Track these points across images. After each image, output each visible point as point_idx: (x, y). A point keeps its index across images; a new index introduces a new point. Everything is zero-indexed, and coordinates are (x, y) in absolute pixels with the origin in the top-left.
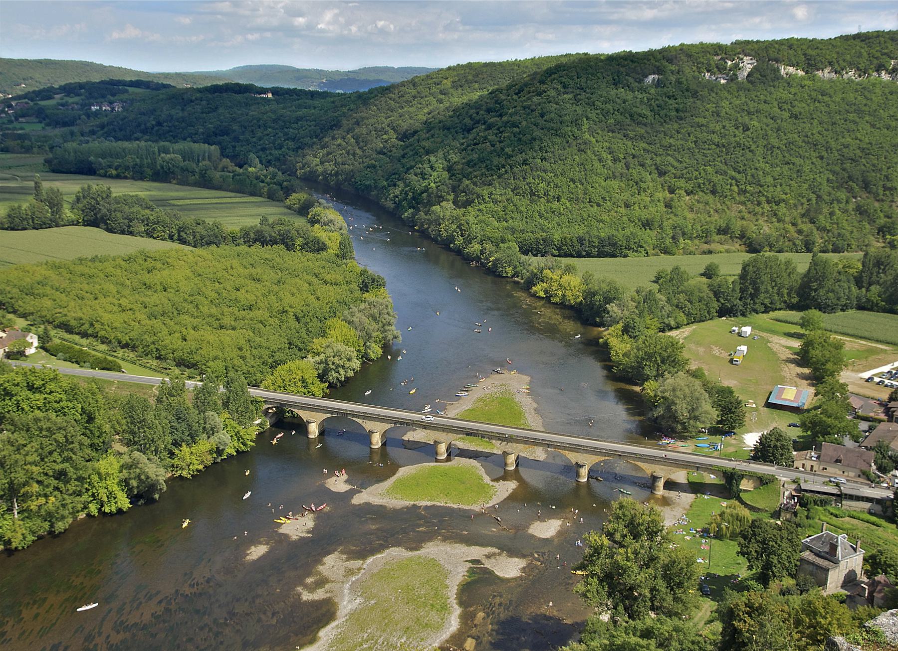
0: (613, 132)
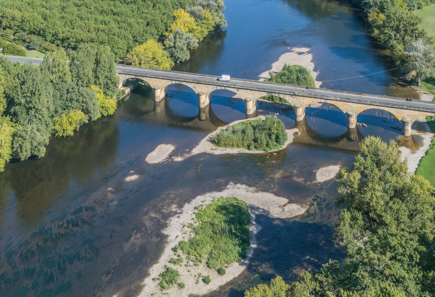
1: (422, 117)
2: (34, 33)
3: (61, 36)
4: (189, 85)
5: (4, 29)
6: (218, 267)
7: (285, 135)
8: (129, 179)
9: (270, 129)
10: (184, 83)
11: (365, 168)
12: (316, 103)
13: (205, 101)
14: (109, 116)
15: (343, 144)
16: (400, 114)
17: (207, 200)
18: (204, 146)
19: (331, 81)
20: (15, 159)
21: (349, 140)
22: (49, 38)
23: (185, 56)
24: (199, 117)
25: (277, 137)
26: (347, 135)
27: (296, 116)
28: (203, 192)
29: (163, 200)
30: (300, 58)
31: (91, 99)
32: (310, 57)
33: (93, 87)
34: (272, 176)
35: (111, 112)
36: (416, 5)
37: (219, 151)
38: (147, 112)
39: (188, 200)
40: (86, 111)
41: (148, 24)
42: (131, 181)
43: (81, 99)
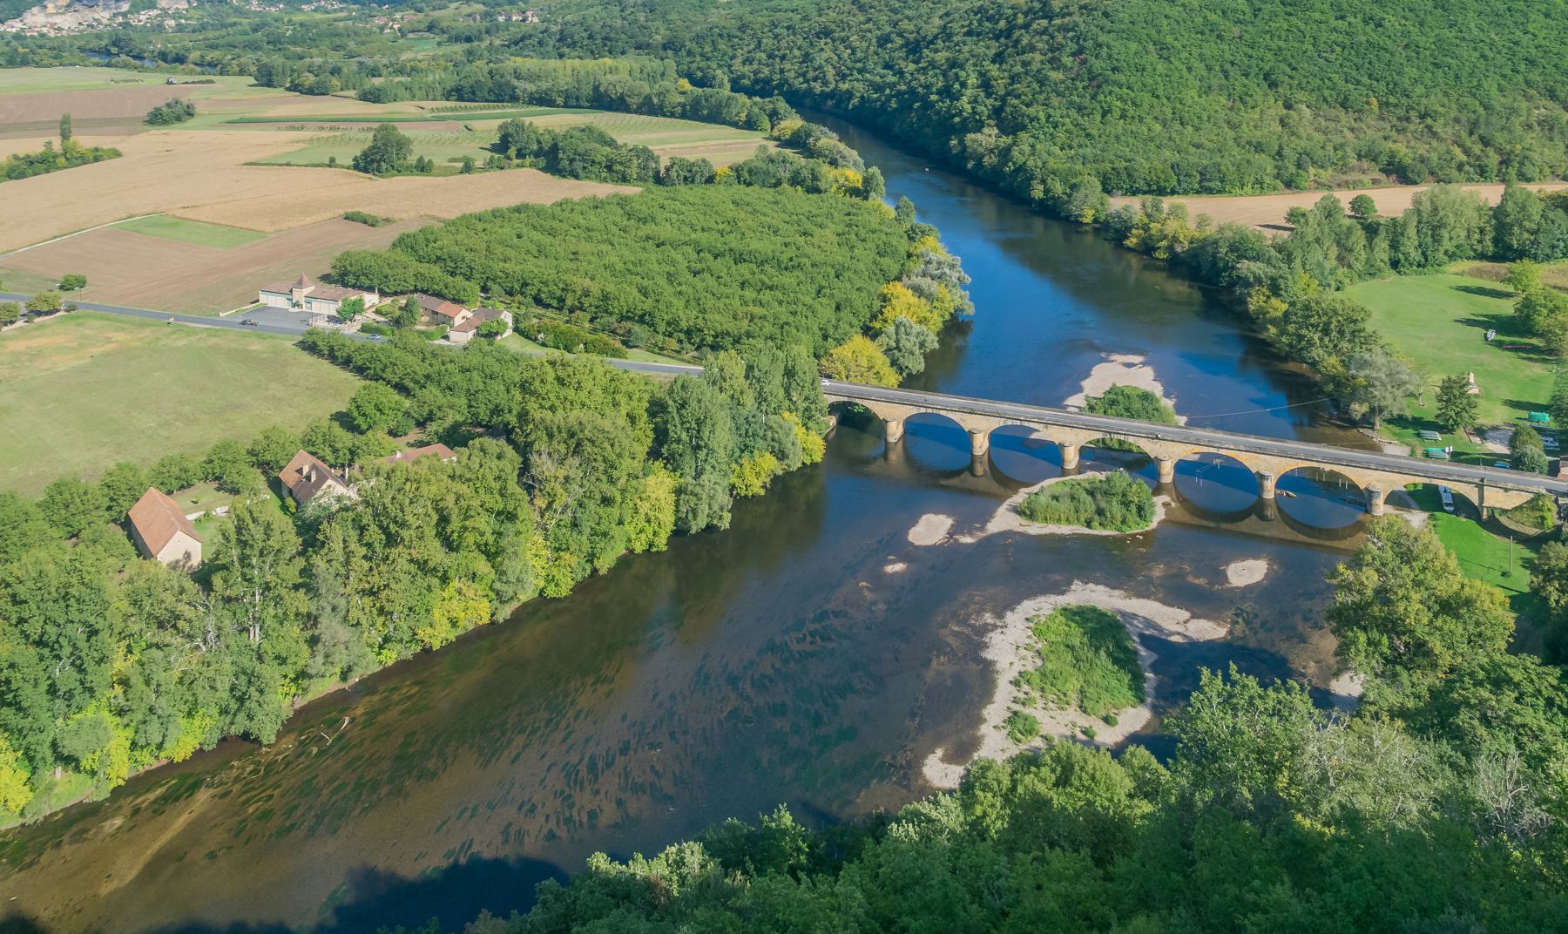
0: (1202, 33)
1: (1400, 482)
2: (629, 318)
3: (684, 325)
4: (951, 415)
5: (571, 311)
6: (1104, 713)
7: (1152, 505)
8: (890, 569)
9: (1124, 495)
10: (942, 413)
11: (1383, 565)
12: (1188, 452)
13: (981, 445)
14: (814, 465)
15: (1251, 524)
16: (1362, 478)
17: (1044, 606)
18: (1003, 520)
19: (1199, 413)
20: (679, 532)
21: (1263, 517)
22: (662, 327)
23: (917, 365)
24: (971, 469)
25: (1140, 509)
26: (1258, 509)
27: (1159, 475)
28: (1031, 594)
29: (965, 605)
30: (1123, 372)
31: (787, 435)
32: (1149, 372)
33: (786, 414)
34: (1146, 572)
35: (818, 458)
36: (1333, 284)
37: (1035, 529)
38: (866, 461)
39: (1011, 605)
40: (781, 455)
41: (838, 308)
42: (896, 573)
43: (769, 434)
